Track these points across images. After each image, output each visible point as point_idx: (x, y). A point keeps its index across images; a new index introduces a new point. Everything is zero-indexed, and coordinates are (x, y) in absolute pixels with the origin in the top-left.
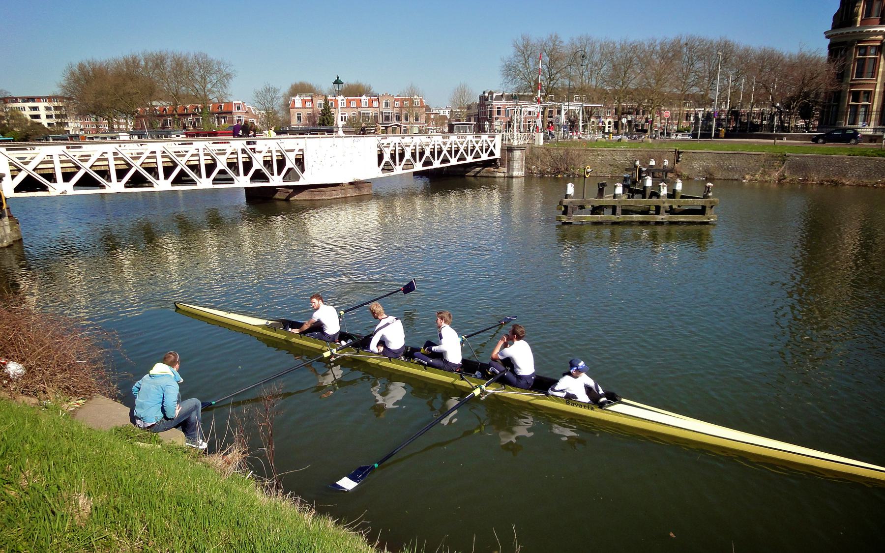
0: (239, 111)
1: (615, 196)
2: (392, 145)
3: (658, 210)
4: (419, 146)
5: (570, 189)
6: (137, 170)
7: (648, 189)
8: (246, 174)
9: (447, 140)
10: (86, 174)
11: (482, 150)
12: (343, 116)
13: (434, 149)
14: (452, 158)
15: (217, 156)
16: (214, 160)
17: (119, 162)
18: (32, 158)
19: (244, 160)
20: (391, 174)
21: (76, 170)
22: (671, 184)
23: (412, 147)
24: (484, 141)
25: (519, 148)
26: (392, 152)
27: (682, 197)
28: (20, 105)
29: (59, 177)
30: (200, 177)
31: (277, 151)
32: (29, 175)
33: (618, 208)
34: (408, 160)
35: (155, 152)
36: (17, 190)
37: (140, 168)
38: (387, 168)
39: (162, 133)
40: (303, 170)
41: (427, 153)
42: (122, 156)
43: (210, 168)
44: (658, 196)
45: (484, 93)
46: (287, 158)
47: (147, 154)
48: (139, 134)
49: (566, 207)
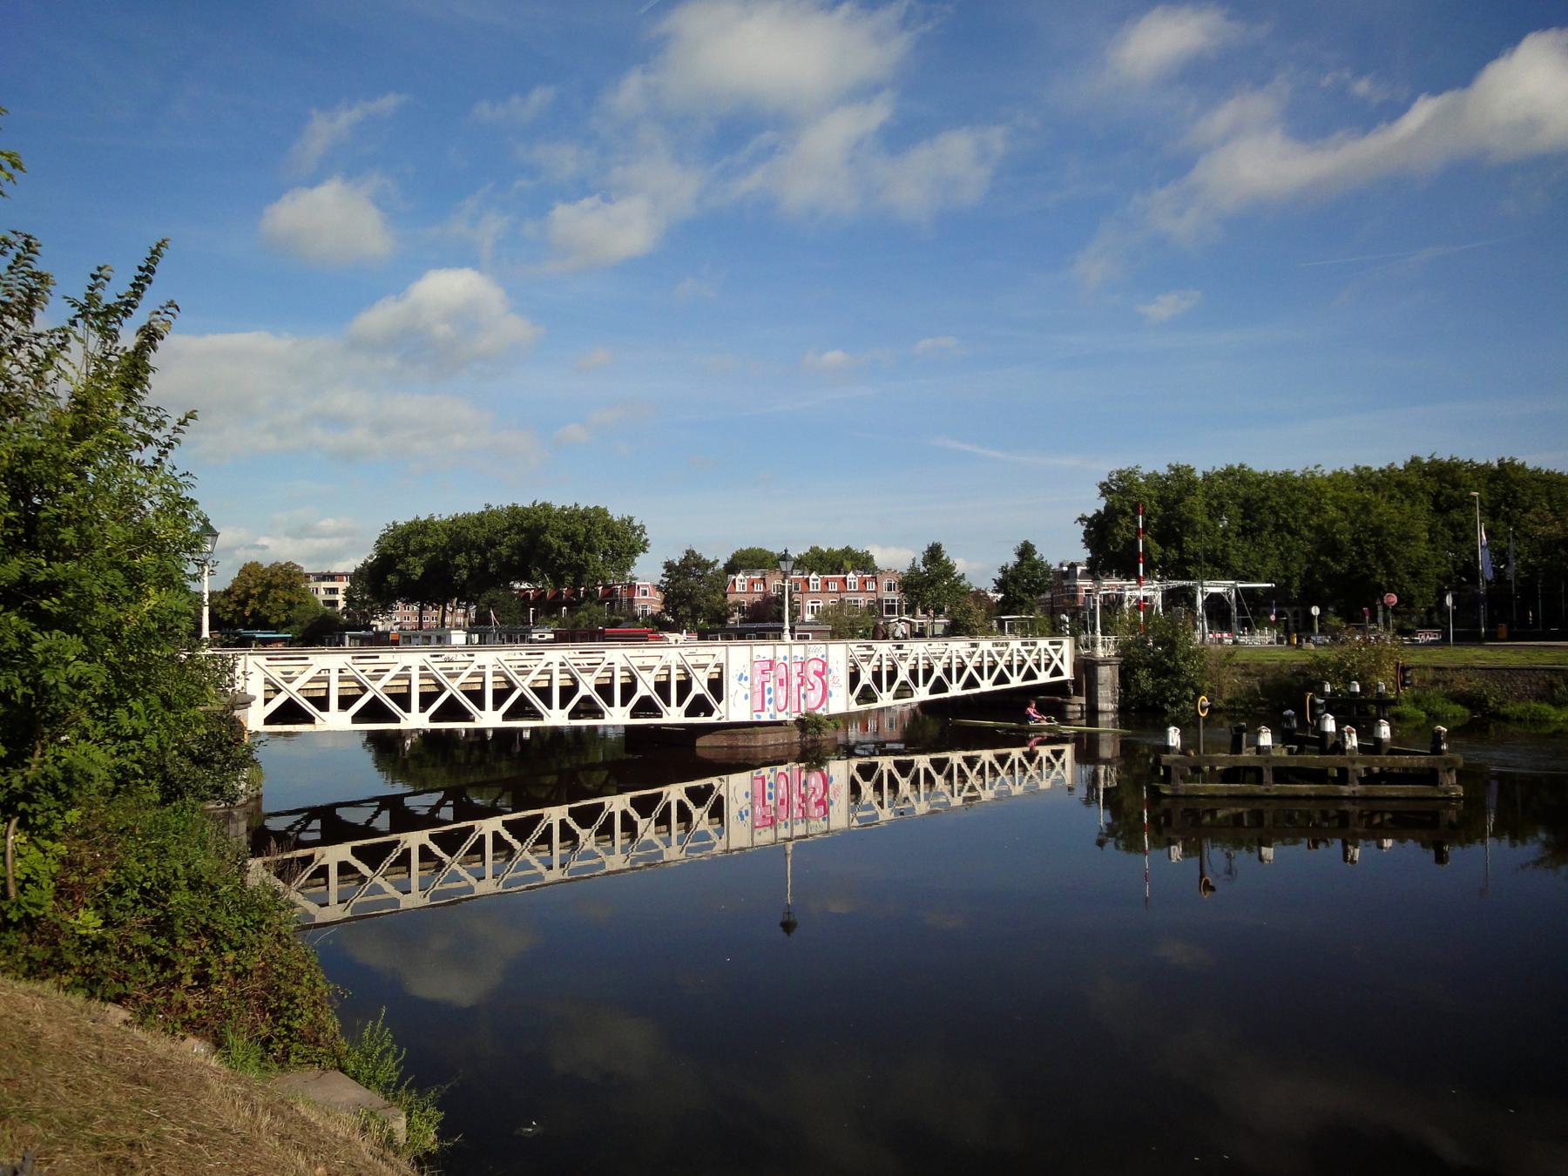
0: (645, 597)
1: (1259, 749)
2: (910, 657)
3: (1343, 777)
4: (495, 674)
5: (1174, 737)
6: (452, 695)
7: (1329, 738)
8: (624, 703)
9: (1005, 648)
10: (375, 700)
11: (1038, 666)
12: (815, 605)
13: (880, 667)
14: (982, 679)
15: (581, 675)
16: (574, 679)
17: (346, 684)
18: (302, 673)
19: (624, 681)
20: (873, 706)
21: (361, 693)
22: (1367, 732)
23: (945, 660)
24: (1043, 651)
25: (1105, 662)
26: (876, 669)
27: (1392, 752)
28: (313, 585)
29: (334, 702)
30: (550, 706)
31: (623, 669)
32: (290, 698)
33: (1265, 772)
34: (904, 683)
35: (484, 667)
36: (269, 720)
37: (381, 692)
38: (867, 696)
39: (515, 634)
40: (719, 698)
41: (938, 672)
42: (352, 673)
43: (567, 693)
44: (1343, 751)
45: (1061, 565)
46: (639, 681)
47: (395, 670)
48: (482, 632)
49: (1167, 769)
